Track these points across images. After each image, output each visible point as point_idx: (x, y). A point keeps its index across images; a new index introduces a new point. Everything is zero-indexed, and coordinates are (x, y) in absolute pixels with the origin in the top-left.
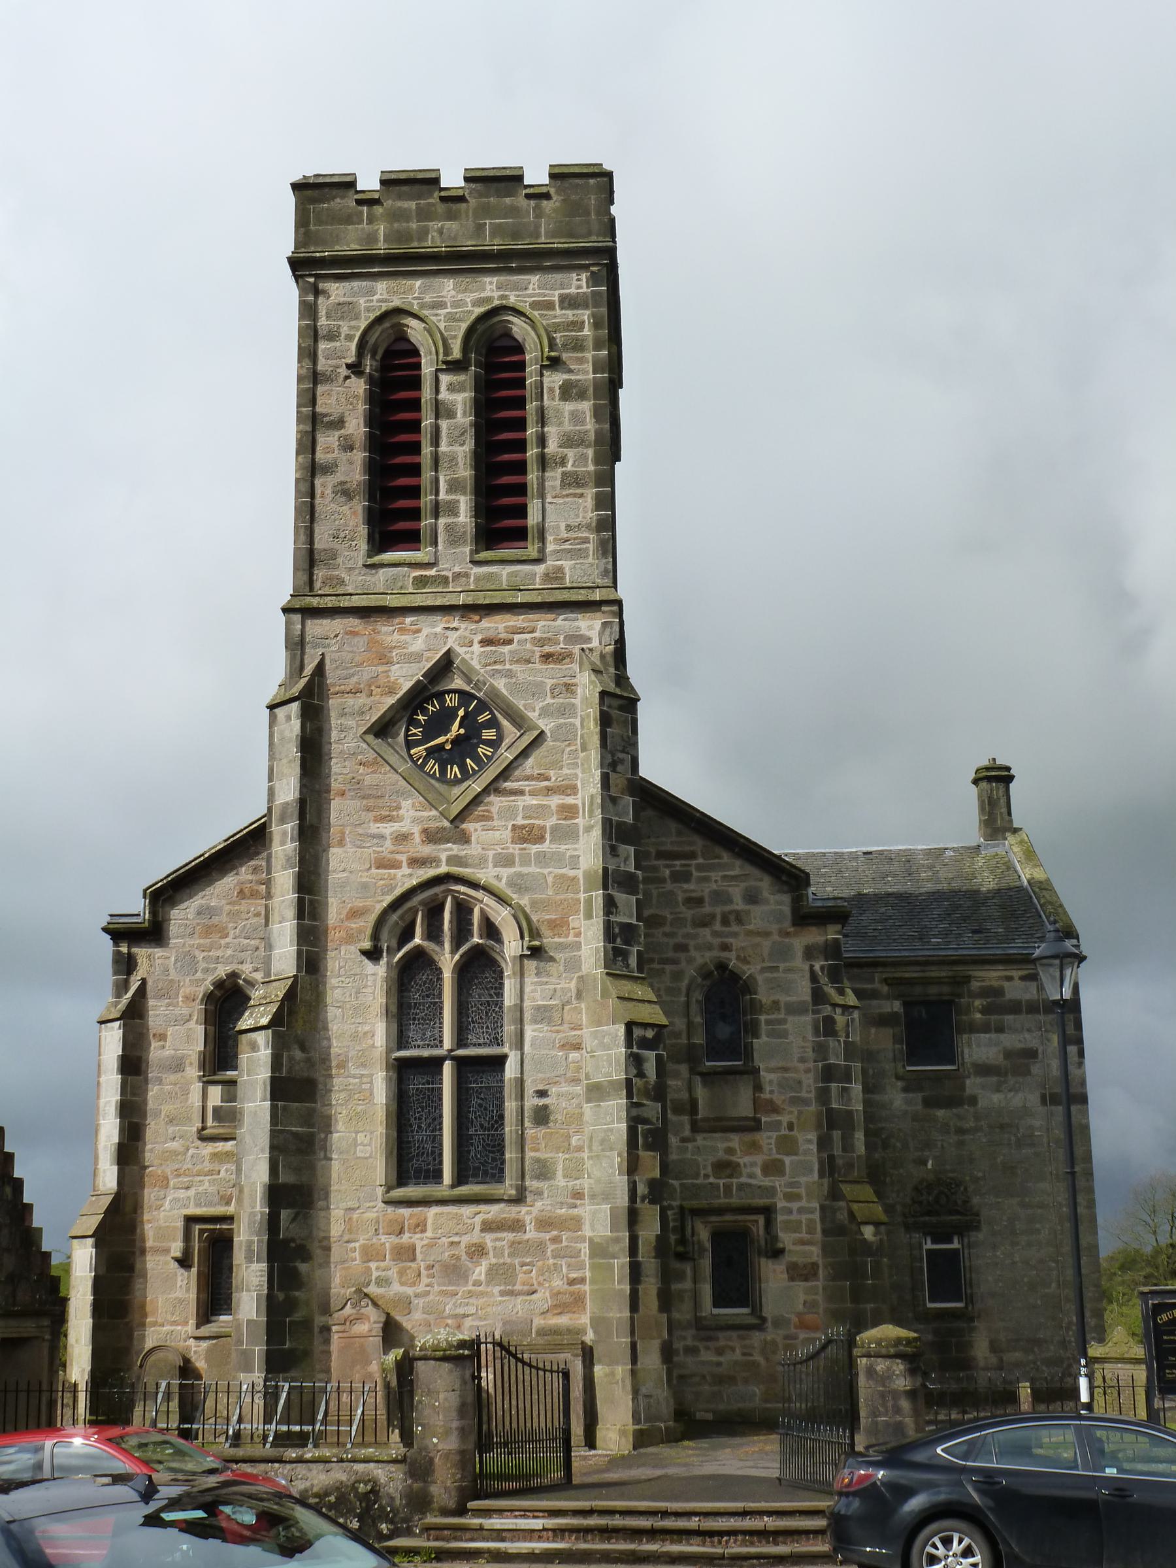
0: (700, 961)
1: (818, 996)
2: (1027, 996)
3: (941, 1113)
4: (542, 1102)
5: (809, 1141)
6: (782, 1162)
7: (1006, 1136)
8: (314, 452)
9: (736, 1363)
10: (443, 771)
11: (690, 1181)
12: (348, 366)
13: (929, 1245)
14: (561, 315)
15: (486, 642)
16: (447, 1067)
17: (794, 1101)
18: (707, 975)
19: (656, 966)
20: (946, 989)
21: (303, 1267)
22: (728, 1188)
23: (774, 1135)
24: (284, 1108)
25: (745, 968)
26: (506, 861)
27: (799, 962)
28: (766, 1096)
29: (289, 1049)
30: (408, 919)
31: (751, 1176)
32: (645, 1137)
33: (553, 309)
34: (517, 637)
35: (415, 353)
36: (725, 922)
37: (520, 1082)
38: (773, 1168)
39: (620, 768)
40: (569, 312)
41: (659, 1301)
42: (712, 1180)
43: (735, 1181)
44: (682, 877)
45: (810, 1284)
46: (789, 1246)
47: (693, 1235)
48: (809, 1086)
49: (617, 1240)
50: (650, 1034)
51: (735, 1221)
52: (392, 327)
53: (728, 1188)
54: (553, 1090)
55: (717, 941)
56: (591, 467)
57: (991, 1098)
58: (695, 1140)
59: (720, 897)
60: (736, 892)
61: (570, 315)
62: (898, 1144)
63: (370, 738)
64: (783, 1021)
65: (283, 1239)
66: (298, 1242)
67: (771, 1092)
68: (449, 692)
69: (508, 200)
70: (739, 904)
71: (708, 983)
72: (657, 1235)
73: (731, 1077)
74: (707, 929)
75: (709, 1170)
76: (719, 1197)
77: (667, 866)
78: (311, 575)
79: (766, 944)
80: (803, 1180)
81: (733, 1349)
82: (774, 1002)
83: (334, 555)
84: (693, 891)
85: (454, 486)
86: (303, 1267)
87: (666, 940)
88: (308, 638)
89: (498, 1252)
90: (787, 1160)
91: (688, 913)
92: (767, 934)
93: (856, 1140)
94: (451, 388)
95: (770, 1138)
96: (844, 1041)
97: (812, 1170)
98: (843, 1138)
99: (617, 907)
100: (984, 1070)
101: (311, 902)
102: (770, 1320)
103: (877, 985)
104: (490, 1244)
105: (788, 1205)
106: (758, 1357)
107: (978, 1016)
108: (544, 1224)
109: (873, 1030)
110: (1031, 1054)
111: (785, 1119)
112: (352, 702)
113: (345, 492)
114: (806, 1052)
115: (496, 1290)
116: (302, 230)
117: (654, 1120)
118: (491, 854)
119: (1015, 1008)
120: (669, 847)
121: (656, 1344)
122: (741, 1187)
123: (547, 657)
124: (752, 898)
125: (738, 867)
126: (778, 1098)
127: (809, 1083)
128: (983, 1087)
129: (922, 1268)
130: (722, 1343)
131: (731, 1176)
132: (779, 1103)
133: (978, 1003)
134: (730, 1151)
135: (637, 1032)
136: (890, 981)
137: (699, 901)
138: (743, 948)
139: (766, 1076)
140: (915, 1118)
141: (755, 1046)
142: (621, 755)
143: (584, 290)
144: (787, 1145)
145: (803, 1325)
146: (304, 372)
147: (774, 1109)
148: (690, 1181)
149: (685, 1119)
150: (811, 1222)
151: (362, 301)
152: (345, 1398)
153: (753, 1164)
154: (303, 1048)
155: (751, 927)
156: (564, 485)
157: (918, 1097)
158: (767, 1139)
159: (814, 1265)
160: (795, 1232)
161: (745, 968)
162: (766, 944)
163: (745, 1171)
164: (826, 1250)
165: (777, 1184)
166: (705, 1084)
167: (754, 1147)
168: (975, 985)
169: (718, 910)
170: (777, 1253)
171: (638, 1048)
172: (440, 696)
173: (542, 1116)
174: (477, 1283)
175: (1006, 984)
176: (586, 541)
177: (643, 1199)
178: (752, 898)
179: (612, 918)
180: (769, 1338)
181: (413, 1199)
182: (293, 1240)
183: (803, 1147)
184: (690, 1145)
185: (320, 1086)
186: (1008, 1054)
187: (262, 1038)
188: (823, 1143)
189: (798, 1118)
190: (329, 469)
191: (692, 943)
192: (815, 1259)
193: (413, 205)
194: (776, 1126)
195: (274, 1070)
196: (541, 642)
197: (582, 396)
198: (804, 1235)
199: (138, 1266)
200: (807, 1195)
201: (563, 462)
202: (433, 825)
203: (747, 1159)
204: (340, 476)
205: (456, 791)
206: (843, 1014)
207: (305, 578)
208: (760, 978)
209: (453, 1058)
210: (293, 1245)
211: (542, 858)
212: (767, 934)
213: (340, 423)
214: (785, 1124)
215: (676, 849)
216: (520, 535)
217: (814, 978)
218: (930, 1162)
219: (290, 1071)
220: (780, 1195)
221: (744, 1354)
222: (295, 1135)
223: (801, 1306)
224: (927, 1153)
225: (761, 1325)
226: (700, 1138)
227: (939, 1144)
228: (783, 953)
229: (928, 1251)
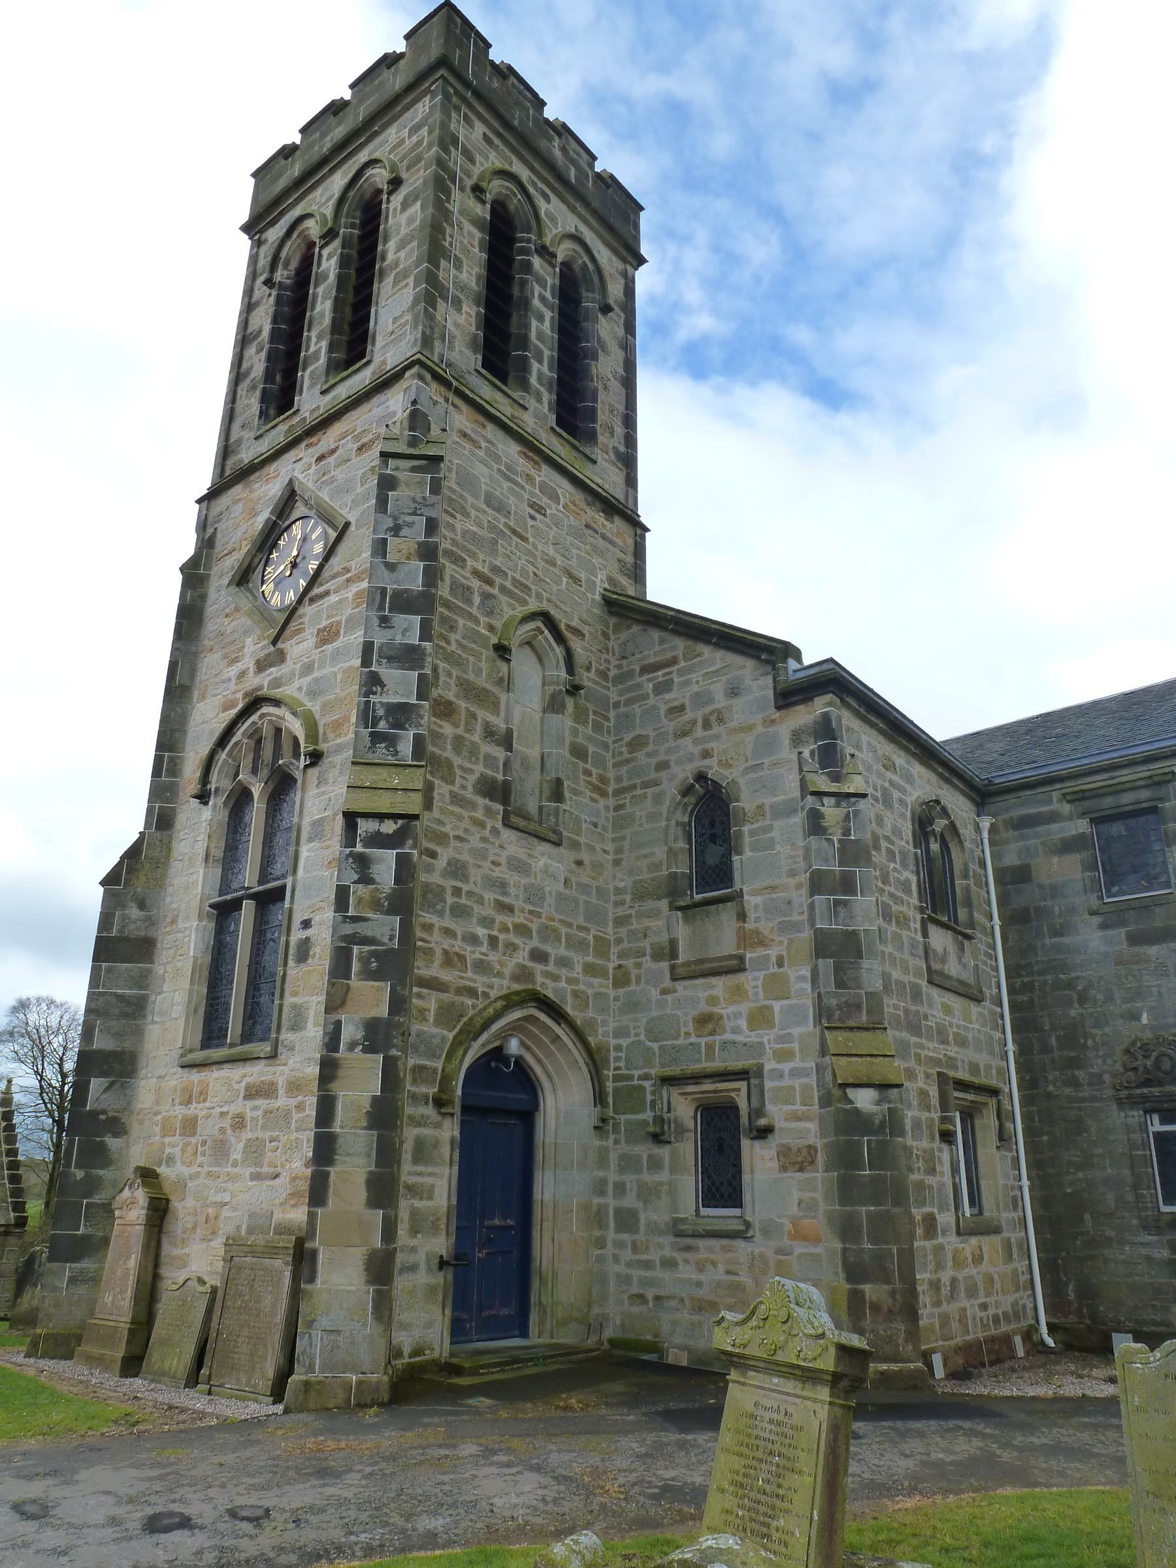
0: (681, 776)
3: (1153, 951)
5: (802, 978)
6: (769, 1008)
9: (718, 1284)
11: (670, 1042)
17: (785, 928)
18: (687, 791)
19: (638, 792)
20: (1145, 794)
21: (112, 1142)
22: (710, 1047)
23: (762, 974)
24: (109, 970)
25: (726, 773)
27: (787, 753)
28: (750, 925)
29: (124, 907)
31: (735, 1031)
32: (365, 961)
36: (707, 725)
38: (760, 1018)
41: (368, 1191)
42: (693, 1039)
43: (717, 1038)
44: (663, 687)
45: (806, 1175)
46: (779, 1124)
47: (669, 1111)
48: (801, 906)
50: (389, 827)
51: (715, 1092)
53: (710, 1047)
55: (697, 750)
58: (675, 991)
59: (701, 699)
60: (718, 689)
62: (1100, 997)
64: (770, 828)
65: (90, 1111)
66: (110, 1114)
67: (757, 920)
70: (721, 701)
71: (691, 799)
72: (375, 1098)
73: (713, 908)
74: (688, 739)
75: (691, 1027)
76: (699, 1061)
77: (649, 680)
79: (749, 739)
80: (796, 1031)
81: (714, 1264)
82: (759, 807)
84: (675, 699)
86: (112, 1142)
87: (648, 760)
90: (777, 1006)
91: (670, 726)
92: (750, 728)
95: (755, 979)
96: (840, 841)
97: (806, 1017)
99: (383, 685)
101: (171, 759)
102: (757, 1226)
103: (1055, 806)
105: (778, 1066)
106: (744, 1278)
111: (773, 953)
114: (796, 862)
115: (248, 1172)
117: (386, 940)
120: (652, 660)
121: (357, 1256)
122: (725, 1045)
124: (734, 692)
126: (766, 927)
130: (703, 1255)
131: (713, 1033)
132: (766, 933)
134: (712, 1001)
135: (365, 827)
136: (1069, 798)
137: (681, 709)
138: (725, 751)
139: (750, 900)
140: (1119, 961)
144: (777, 987)
145: (799, 1235)
147: (761, 941)
148: (670, 1042)
150: (806, 1088)
153: (737, 1015)
154: (142, 905)
155: (732, 725)
157: (1120, 933)
158: (752, 980)
159: (811, 1149)
160: (787, 1103)
161: (726, 773)
162: (749, 739)
163: (729, 1025)
165: (765, 1040)
166: (686, 920)
167: (738, 993)
169: (699, 715)
170: (764, 1133)
171: (365, 846)
177: (352, 1046)
178: (734, 692)
179: (373, 698)
180: (757, 1251)
181: (197, 1062)
182: (104, 1112)
183: (796, 986)
184: (669, 998)
185: (159, 945)
189: (788, 949)
191: (673, 758)
192: (812, 1140)
194: (763, 962)
195: (100, 929)
198: (798, 1107)
200: (801, 1051)
203: (731, 1009)
206: (838, 805)
208: (742, 782)
210: (103, 1117)
212: (750, 728)
214: (774, 959)
215: (658, 659)
218: (1145, 1016)
219: (120, 931)
220: (769, 1053)
221: (728, 1272)
222: (121, 998)
223: (795, 1208)
224: (1139, 1004)
225: (742, 1234)
226: (680, 986)
227: (1155, 990)
228: (767, 746)
229: (1159, 1136)
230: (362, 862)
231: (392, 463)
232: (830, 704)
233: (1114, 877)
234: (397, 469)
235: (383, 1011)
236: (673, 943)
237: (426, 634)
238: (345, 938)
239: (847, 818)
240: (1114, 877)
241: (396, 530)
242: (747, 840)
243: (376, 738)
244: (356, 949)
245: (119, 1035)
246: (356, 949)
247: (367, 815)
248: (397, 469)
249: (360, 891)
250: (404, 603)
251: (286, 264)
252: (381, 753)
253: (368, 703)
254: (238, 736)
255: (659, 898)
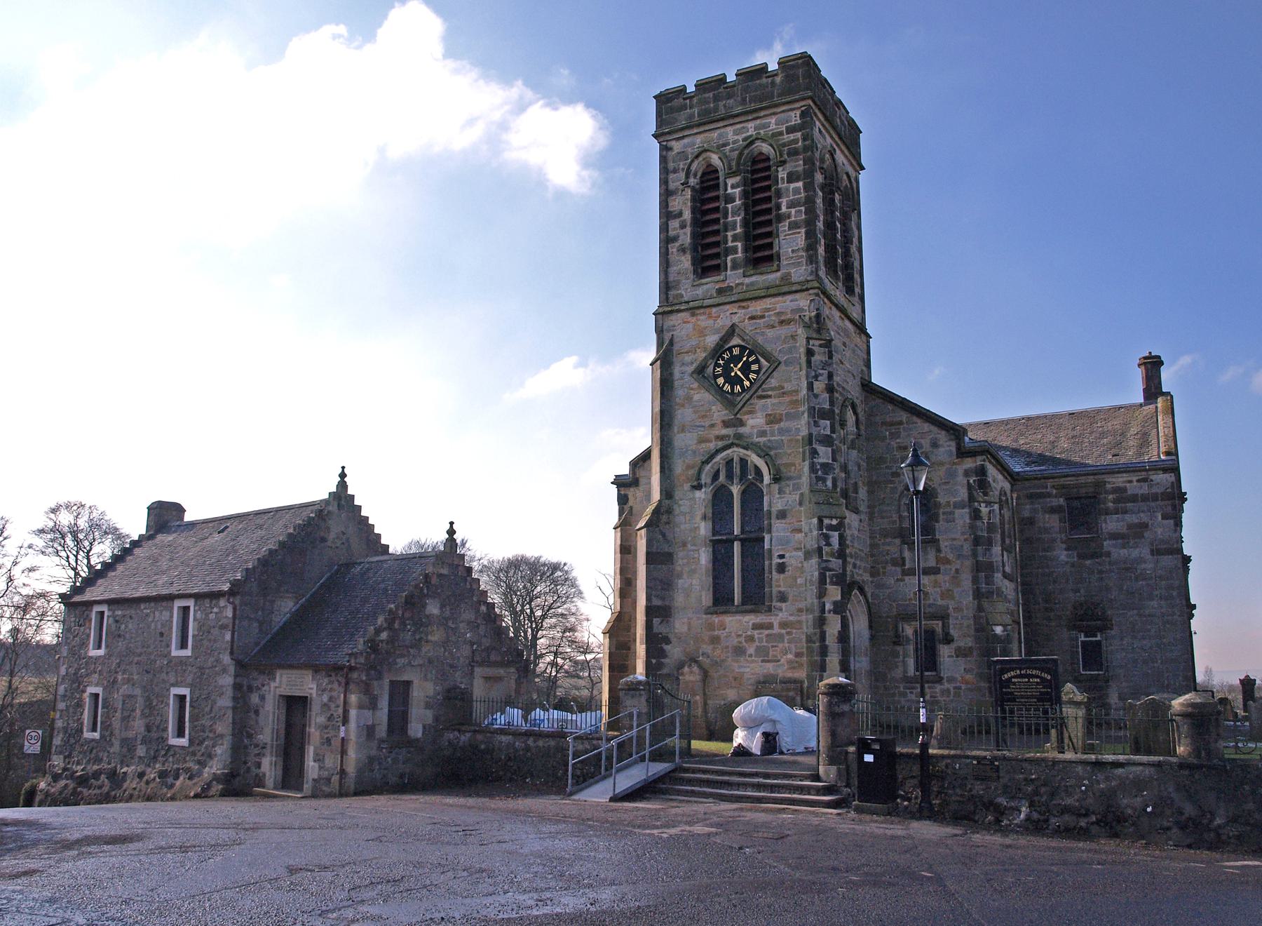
1: (971, 498)
2: (1142, 492)
3: (1088, 562)
4: (781, 561)
7: (1129, 574)
8: (668, 231)
10: (732, 389)
12: (682, 184)
13: (1082, 638)
14: (787, 138)
15: (752, 318)
16: (736, 544)
17: (959, 557)
21: (667, 647)
26: (762, 433)
27: (961, 479)
30: (716, 468)
32: (831, 579)
33: (783, 135)
34: (766, 314)
35: (717, 171)
37: (770, 551)
39: (820, 378)
40: (791, 135)
44: (894, 436)
47: (903, 632)
49: (815, 634)
50: (834, 522)
52: (704, 159)
54: (787, 555)
56: (804, 216)
57: (1119, 553)
61: (792, 136)
63: (695, 376)
68: (734, 347)
69: (758, 82)
78: (667, 294)
83: (678, 282)
85: (735, 238)
88: (665, 327)
89: (761, 640)
93: (995, 579)
94: (733, 187)
98: (986, 577)
100: (1114, 536)
104: (756, 636)
107: (1111, 504)
108: (783, 625)
109: (1047, 516)
110: (1144, 526)
112: (688, 358)
113: (682, 250)
116: (659, 120)
118: (755, 431)
119: (1134, 498)
123: (782, 322)
125: (926, 427)
126: (950, 556)
127: (967, 548)
128: (1115, 546)
129: (1077, 652)
133: (1111, 497)
139: (943, 544)
140: (1073, 565)
141: (937, 527)
142: (821, 372)
143: (799, 121)
146: (662, 191)
147: (948, 562)
149: (899, 569)
151: (689, 149)
152: (491, 703)
156: (790, 229)
164: (977, 639)
168: (1108, 486)
170: (948, 640)
172: (730, 349)
173: (782, 568)
174: (751, 656)
175: (1128, 485)
176: (802, 257)
177: (829, 611)
178: (935, 445)
182: (661, 634)
186: (1130, 527)
187: (643, 532)
188: (975, 580)
190: (675, 239)
192: (970, 645)
193: (711, 95)
196: (779, 314)
197: (797, 180)
199: (632, 647)
201: (789, 217)
202: (726, 418)
204: (680, 242)
205: (739, 399)
207: (665, 296)
209: (741, 540)
211: (781, 432)
213: (680, 214)
216: (770, 259)
217: (969, 486)
225: (939, 680)
226: (907, 578)
229: (1082, 642)
230: (827, 537)
231: (811, 342)
232: (984, 461)
233: (1074, 527)
234: (813, 345)
235: (839, 598)
236: (903, 559)
237: (833, 431)
238: (823, 569)
239: (990, 512)
240: (1074, 527)
241: (816, 377)
242: (941, 517)
243: (818, 479)
244: (827, 573)
245: (663, 599)
246: (827, 573)
247: (826, 517)
248: (813, 345)
249: (826, 549)
250: (824, 414)
251: (695, 175)
252: (820, 485)
253: (813, 462)
254: (718, 458)
255: (895, 538)
